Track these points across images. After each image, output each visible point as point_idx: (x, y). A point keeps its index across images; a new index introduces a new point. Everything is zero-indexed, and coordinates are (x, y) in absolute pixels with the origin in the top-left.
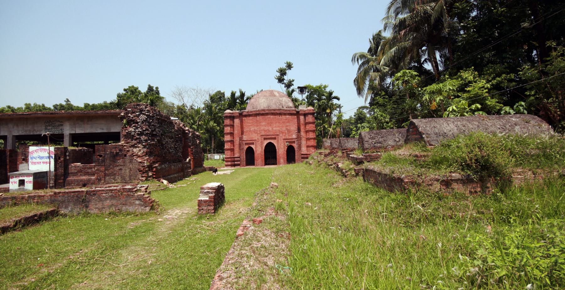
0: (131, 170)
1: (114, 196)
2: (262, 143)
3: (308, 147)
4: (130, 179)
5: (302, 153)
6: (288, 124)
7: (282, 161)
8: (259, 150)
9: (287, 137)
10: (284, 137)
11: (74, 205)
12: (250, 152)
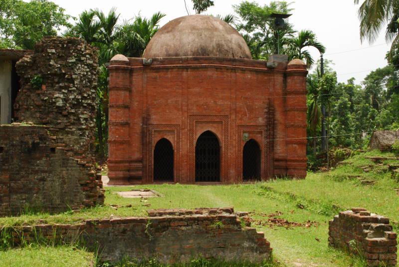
0: (64, 182)
1: (202, 233)
2: (191, 131)
3: (287, 143)
4: (63, 202)
5: (276, 156)
6: (248, 94)
7: (232, 172)
8: (184, 149)
9: (246, 121)
10: (238, 122)
11: (127, 247)
12: (164, 151)
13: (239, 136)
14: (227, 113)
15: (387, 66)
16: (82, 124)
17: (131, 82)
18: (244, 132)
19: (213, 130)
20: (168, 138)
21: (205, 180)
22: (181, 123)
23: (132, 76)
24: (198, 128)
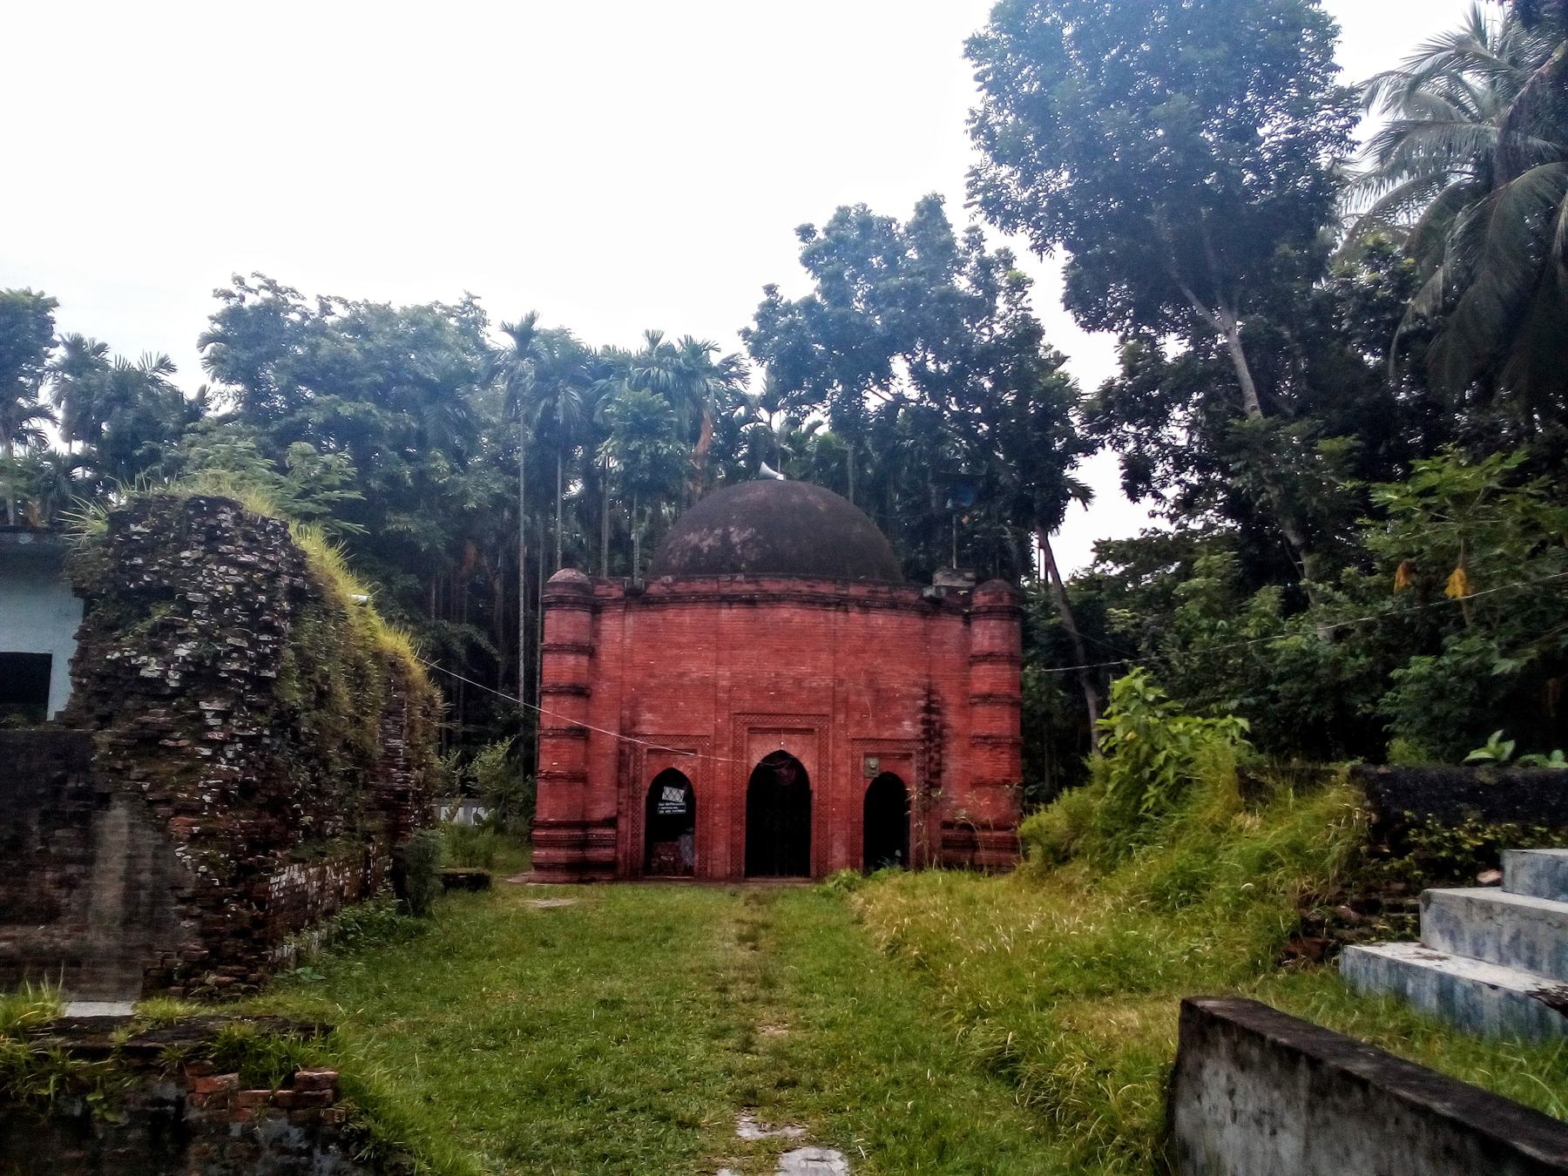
7: (839, 853)
10: (853, 731)
13: (855, 767)
14: (826, 710)
15: (687, 368)
16: (210, 728)
17: (596, 633)
18: (867, 755)
19: (793, 751)
20: (681, 769)
21: (90, 996)
22: (712, 732)
23: (599, 620)
24: (754, 746)
